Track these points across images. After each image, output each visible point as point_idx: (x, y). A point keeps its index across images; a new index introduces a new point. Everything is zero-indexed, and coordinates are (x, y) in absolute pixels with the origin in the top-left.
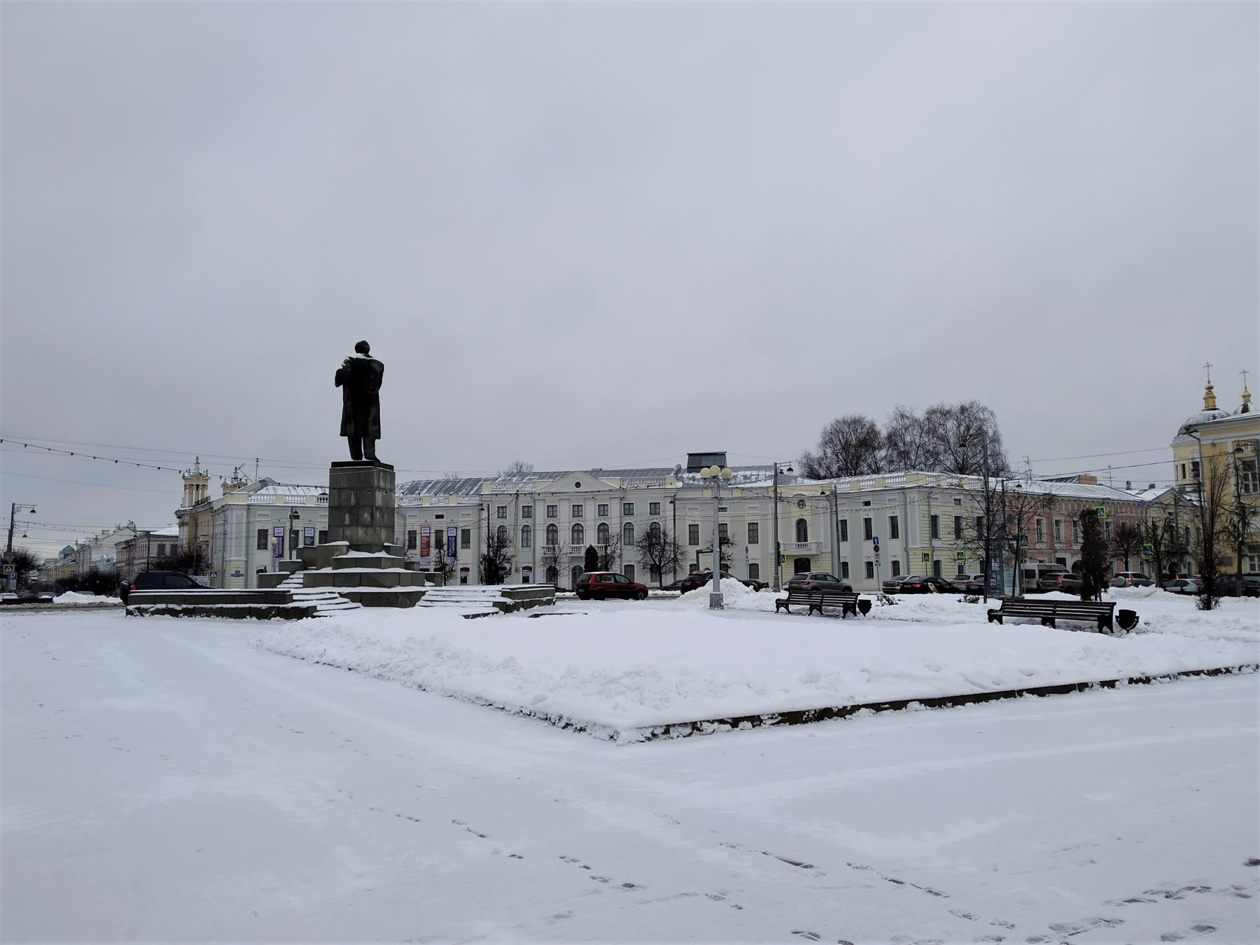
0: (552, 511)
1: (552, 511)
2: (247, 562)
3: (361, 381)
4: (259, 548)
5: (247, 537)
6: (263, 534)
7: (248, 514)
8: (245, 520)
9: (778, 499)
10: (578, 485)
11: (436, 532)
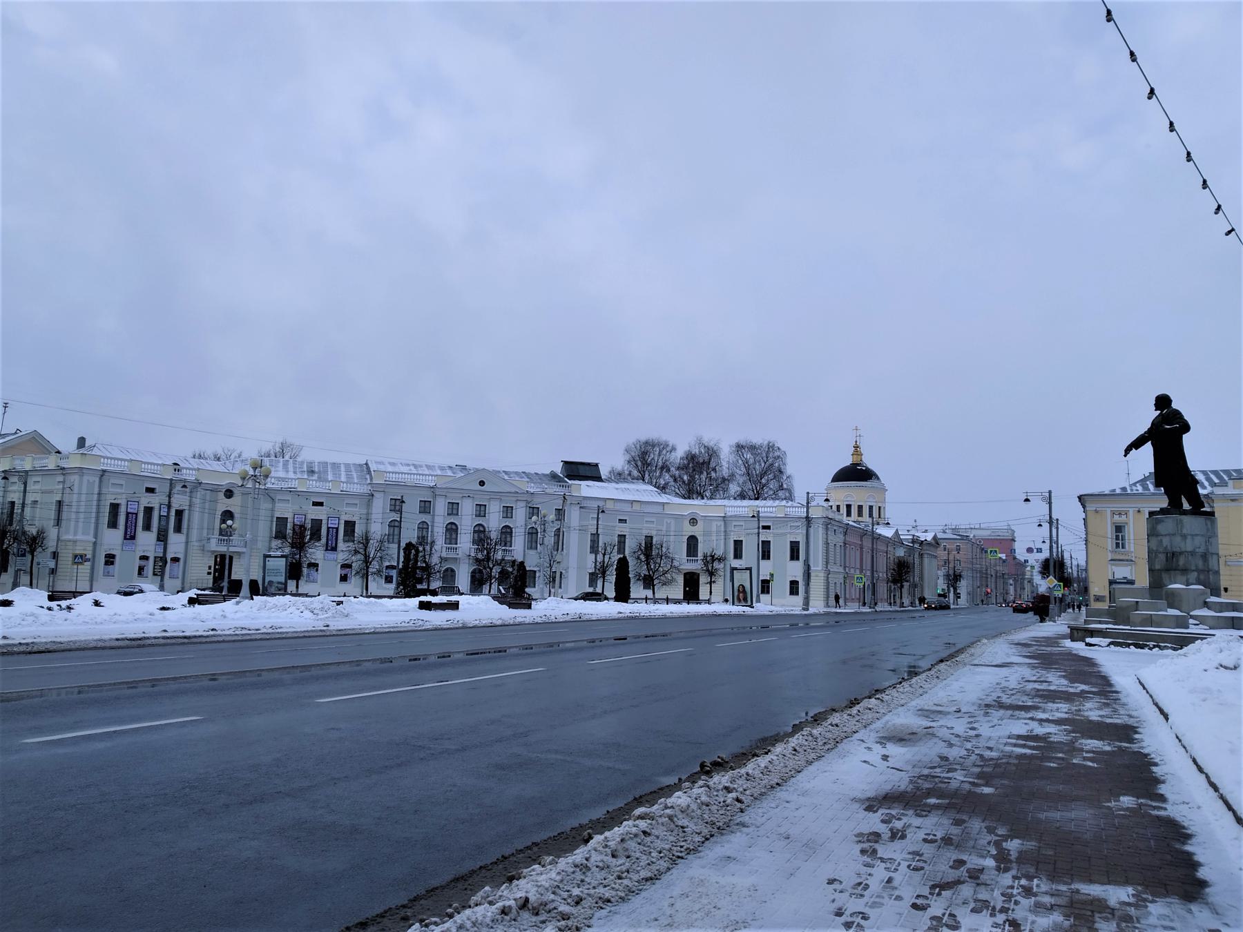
0: (453, 508)
1: (453, 508)
2: (95, 543)
3: (1167, 431)
4: (109, 527)
5: (98, 512)
6: (115, 508)
7: (101, 481)
8: (96, 491)
9: (808, 519)
10: (482, 483)
11: (346, 522)
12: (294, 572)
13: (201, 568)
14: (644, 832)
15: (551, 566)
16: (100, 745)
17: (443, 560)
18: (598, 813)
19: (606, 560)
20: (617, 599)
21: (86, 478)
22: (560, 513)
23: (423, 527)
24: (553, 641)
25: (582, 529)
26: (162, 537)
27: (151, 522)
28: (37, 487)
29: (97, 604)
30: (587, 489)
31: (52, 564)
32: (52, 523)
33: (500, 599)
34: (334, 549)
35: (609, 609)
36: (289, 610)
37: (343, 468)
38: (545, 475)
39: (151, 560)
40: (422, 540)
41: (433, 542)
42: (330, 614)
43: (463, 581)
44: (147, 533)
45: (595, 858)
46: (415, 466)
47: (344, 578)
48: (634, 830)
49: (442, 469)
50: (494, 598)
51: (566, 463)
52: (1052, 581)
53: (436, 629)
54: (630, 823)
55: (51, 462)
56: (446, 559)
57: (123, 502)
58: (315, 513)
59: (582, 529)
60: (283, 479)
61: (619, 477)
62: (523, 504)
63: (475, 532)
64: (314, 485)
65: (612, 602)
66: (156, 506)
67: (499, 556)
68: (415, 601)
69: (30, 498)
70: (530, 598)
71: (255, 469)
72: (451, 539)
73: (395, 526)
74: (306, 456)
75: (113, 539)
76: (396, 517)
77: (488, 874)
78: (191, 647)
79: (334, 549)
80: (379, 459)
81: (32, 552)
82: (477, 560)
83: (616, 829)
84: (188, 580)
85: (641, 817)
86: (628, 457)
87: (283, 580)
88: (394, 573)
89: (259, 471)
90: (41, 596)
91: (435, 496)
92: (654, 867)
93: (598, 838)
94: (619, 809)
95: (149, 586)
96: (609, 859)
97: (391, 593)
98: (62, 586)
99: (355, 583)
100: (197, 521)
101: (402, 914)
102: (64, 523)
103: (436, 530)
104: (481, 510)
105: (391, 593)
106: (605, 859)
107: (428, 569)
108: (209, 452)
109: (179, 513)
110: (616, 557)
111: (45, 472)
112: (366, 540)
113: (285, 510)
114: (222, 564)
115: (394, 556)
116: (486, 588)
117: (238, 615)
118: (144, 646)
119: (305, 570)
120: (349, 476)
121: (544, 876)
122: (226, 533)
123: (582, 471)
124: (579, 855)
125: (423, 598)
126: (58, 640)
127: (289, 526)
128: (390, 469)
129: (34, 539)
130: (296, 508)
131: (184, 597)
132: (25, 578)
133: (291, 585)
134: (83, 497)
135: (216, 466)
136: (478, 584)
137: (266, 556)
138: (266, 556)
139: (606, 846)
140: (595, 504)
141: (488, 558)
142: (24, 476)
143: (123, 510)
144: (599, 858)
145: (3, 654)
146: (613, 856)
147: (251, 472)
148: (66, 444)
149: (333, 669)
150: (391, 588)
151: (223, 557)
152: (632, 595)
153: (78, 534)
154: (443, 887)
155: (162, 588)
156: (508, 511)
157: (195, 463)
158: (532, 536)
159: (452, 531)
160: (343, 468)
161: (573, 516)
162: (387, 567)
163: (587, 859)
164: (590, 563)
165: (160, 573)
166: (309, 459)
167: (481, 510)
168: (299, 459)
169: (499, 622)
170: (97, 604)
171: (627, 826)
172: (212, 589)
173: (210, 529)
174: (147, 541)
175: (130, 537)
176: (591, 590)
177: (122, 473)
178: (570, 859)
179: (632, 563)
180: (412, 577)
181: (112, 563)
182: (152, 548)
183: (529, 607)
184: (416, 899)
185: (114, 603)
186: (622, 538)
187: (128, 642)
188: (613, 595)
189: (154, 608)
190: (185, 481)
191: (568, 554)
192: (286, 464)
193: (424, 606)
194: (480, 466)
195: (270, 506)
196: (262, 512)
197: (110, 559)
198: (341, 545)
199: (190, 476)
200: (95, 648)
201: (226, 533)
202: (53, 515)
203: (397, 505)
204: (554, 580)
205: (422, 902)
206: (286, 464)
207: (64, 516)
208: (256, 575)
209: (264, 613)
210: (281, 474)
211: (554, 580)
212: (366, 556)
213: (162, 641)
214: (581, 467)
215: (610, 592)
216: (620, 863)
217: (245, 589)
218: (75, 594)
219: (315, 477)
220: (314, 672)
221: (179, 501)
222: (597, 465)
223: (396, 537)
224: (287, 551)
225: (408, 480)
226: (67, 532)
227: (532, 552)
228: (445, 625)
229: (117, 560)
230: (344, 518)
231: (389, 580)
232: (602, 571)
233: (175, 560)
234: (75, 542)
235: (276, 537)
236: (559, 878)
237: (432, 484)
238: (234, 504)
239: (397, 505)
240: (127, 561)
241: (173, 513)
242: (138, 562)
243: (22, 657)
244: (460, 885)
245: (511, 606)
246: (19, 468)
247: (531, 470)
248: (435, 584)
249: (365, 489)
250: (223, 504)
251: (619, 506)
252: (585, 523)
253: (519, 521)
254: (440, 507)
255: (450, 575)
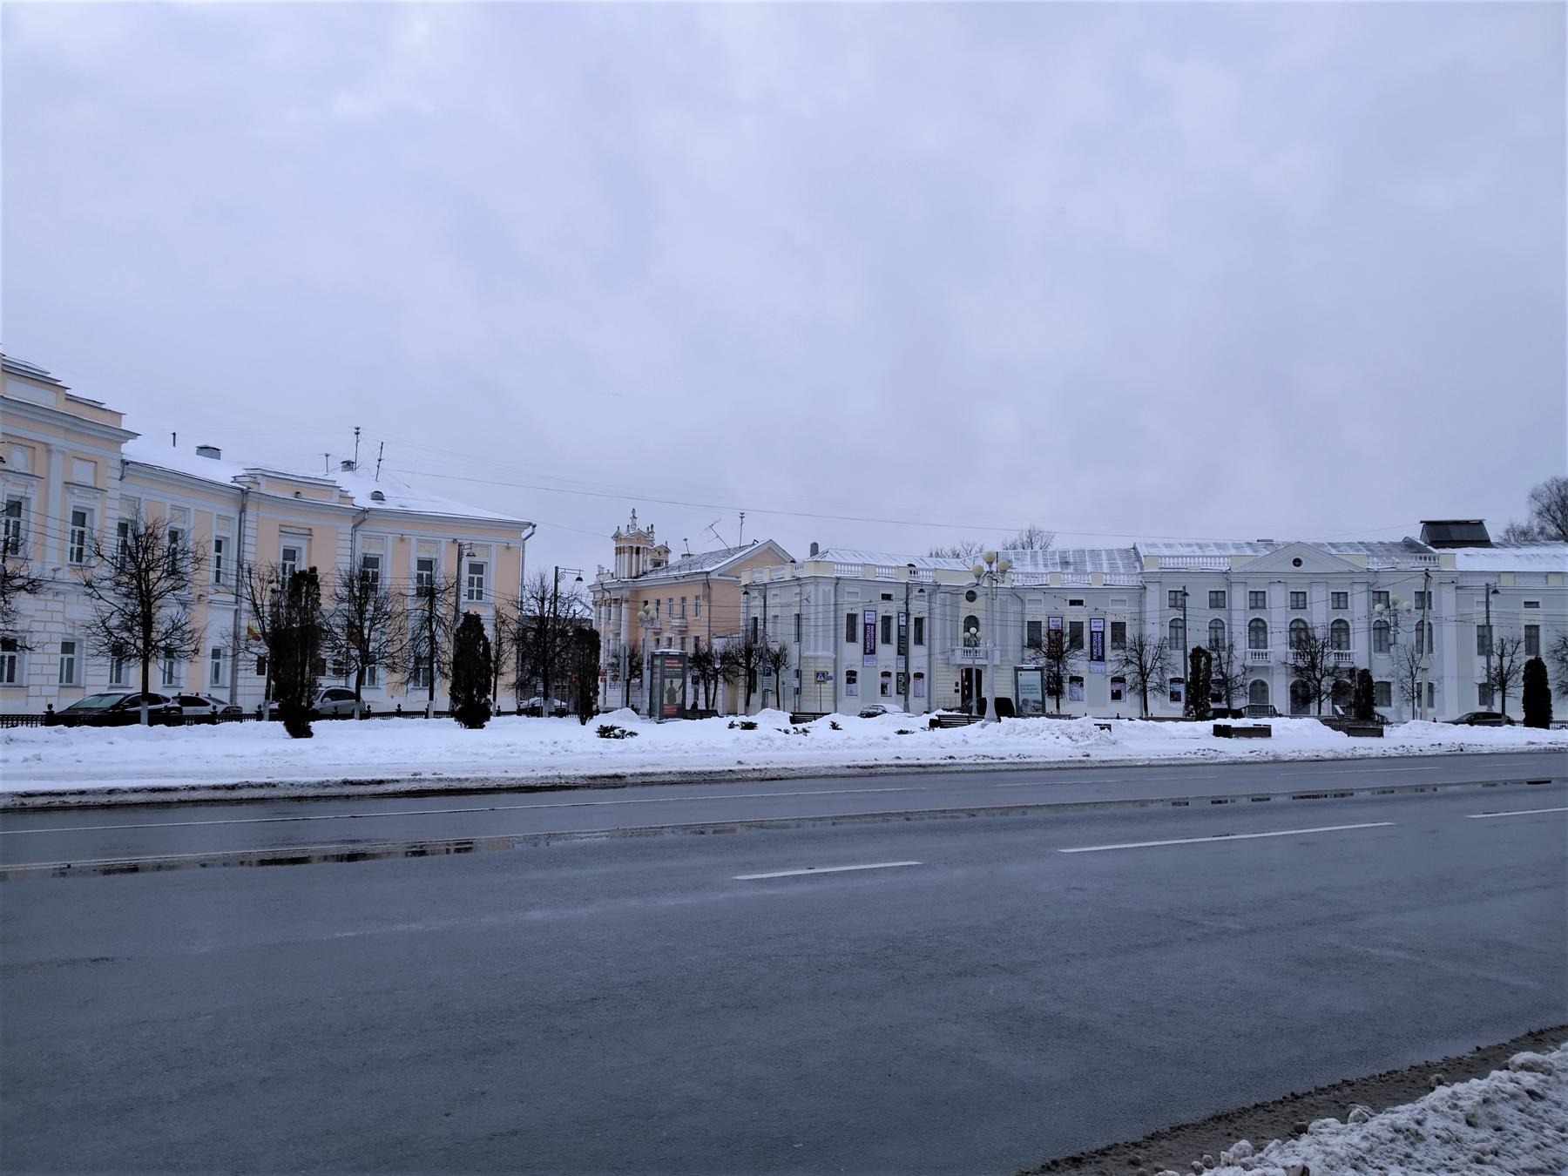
0: (1258, 599)
1: (1258, 599)
6: (852, 618)
10: (1297, 562)
12: (1054, 687)
13: (946, 687)
14: (1531, 1093)
15: (1413, 676)
16: (805, 888)
17: (1247, 669)
18: (1463, 1049)
19: (1506, 664)
20: (1528, 723)
21: (821, 588)
22: (1423, 599)
23: (1216, 625)
24: (1421, 781)
25: (1461, 620)
26: (903, 651)
27: (891, 631)
28: (777, 600)
29: (834, 726)
30: (1465, 559)
31: (796, 684)
32: (793, 638)
33: (1333, 723)
34: (1101, 659)
35: (1516, 737)
36: (1043, 735)
37: (1104, 556)
38: (1394, 544)
39: (894, 676)
40: (1216, 643)
41: (1231, 646)
42: (1092, 740)
43: (1279, 696)
44: (886, 646)
45: (1433, 1122)
46: (1200, 546)
47: (1116, 696)
48: (1510, 1087)
49: (1237, 546)
50: (1326, 722)
51: (1428, 523)
52: (168, 625)
53: (1235, 763)
54: (1504, 1074)
55: (787, 573)
56: (1252, 669)
57: (859, 611)
58: (1073, 614)
59: (1461, 620)
60: (1032, 575)
61: (1522, 537)
62: (1364, 588)
63: (1292, 630)
64: (1069, 580)
65: (1520, 728)
66: (895, 615)
67: (1330, 662)
68: (1209, 725)
69: (771, 613)
70: (1384, 721)
71: (990, 563)
72: (1257, 641)
73: (1178, 626)
74: (1058, 544)
75: (853, 653)
76: (1179, 614)
77: (1266, 1117)
78: (924, 778)
79: (1101, 659)
80: (1149, 541)
81: (777, 671)
82: (1297, 669)
83: (1474, 1081)
84: (934, 699)
85: (1525, 1067)
86: (1537, 506)
87: (1039, 698)
88: (1181, 688)
89: (996, 568)
90: (783, 718)
91: (1230, 584)
92: (1548, 1154)
93: (1442, 1091)
94: (1500, 1047)
95: (892, 705)
96: (1461, 1129)
97: (1180, 714)
98: (808, 707)
99: (1130, 702)
100: (937, 629)
101: (1132, 1155)
102: (804, 638)
103: (1234, 629)
104: (1299, 600)
105: (1180, 714)
106: (1453, 1126)
107: (1225, 682)
108: (947, 549)
109: (919, 621)
110: (1522, 659)
111: (782, 584)
112: (1140, 647)
113: (853, 603)
114: (971, 680)
115: (1178, 665)
116: (1313, 707)
117: (982, 740)
118: (876, 775)
119: (1066, 686)
120: (1113, 566)
121: (1340, 1139)
122: (971, 643)
123: (1456, 534)
124: (1403, 1114)
125: (1220, 721)
126: (650, 770)
127: (1044, 631)
128: (1165, 552)
129: (777, 657)
130: (1051, 609)
131: (926, 719)
132: (772, 699)
133: (1050, 705)
134: (820, 609)
135: (956, 564)
136: (1301, 701)
137: (1017, 670)
138: (1017, 670)
139: (1455, 1106)
140: (1482, 582)
141: (1313, 666)
142: (764, 588)
143: (860, 620)
144: (1441, 1123)
145: (6, 810)
146: (1469, 1124)
147: (986, 568)
148: (801, 553)
149: (1070, 813)
150: (1178, 708)
151: (969, 671)
152: (1555, 716)
153: (820, 649)
154: (1196, 1127)
155: (906, 709)
156: (1340, 599)
157: (931, 563)
158: (1382, 633)
159: (1258, 630)
160: (1104, 556)
161: (1445, 602)
162: (1172, 681)
163: (1419, 1123)
164: (1478, 669)
165: (903, 689)
166: (1062, 547)
167: (1299, 600)
168: (1050, 549)
169: (1329, 755)
170: (834, 726)
171: (1498, 1078)
172: (961, 710)
173: (954, 638)
174: (887, 655)
175: (870, 651)
176: (1484, 709)
177: (856, 580)
178: (1386, 1118)
179: (1551, 668)
180: (1205, 691)
181: (854, 681)
182: (893, 663)
183: (1380, 734)
184: (1154, 1137)
185: (853, 725)
186: (1532, 631)
187: (18, 801)
188: (1521, 716)
189: (890, 731)
190: (922, 584)
191: (1441, 656)
192: (1034, 557)
193: (1220, 731)
194: (1293, 540)
195: (1019, 608)
196: (1011, 617)
197: (851, 677)
198: (1109, 654)
199: (926, 578)
200: (826, 776)
201: (971, 643)
202: (793, 629)
203: (1178, 599)
204: (1419, 696)
205: (1164, 1143)
206: (1034, 557)
207: (804, 630)
208: (1007, 692)
209: (1013, 739)
210: (1030, 569)
211: (1422, 696)
212: (1142, 667)
213: (895, 770)
214: (1452, 528)
215: (1516, 711)
216: (1481, 1137)
217: (991, 709)
218: (815, 716)
219: (1071, 569)
220: (1031, 815)
221: (918, 608)
222: (1480, 523)
223: (1181, 642)
224: (1043, 662)
225: (1192, 564)
226: (808, 649)
227: (1382, 656)
228: (1249, 757)
229: (859, 678)
230: (1110, 619)
231: (1175, 697)
232: (1496, 683)
233: (919, 676)
234: (816, 658)
235: (1029, 646)
236: (1365, 1145)
237: (1224, 569)
238: (978, 608)
239: (1178, 599)
240: (869, 678)
241: (912, 622)
242: (880, 680)
243: (757, 784)
244: (1222, 1127)
245: (1351, 732)
246: (758, 581)
247: (1373, 538)
248: (1240, 703)
249: (1135, 581)
250: (966, 609)
251: (1522, 583)
252: (1467, 610)
253: (1359, 611)
254: (1239, 598)
255: (1259, 690)
